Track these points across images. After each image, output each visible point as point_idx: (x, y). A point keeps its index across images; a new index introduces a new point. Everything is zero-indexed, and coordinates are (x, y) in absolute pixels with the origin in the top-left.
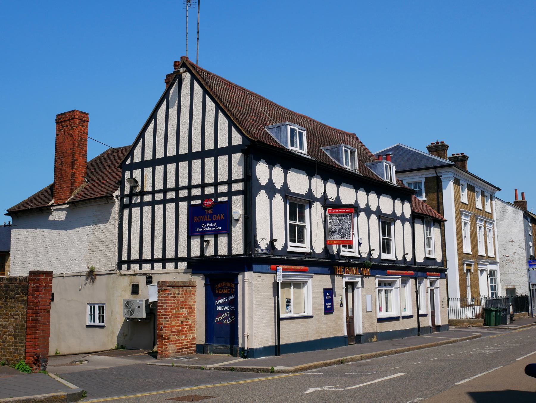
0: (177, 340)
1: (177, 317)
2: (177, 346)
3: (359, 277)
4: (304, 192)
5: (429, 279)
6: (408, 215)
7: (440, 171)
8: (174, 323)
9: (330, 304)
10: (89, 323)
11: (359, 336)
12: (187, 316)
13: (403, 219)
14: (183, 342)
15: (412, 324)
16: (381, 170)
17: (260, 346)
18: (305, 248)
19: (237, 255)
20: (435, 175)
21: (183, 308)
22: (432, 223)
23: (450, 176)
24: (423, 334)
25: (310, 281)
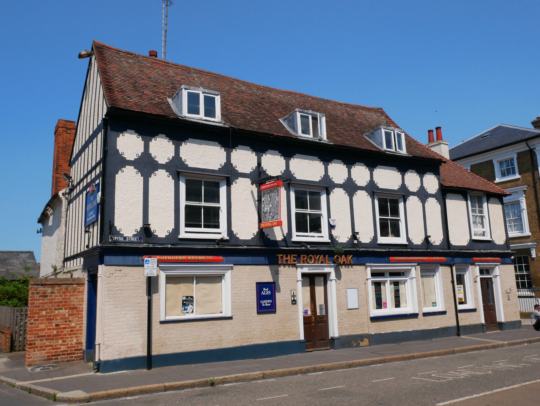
0: (47, 346)
1: (47, 320)
2: (47, 353)
3: (331, 267)
4: (396, 187)
5: (479, 265)
7: (532, 143)
8: (42, 326)
10: (162, 319)
11: (333, 339)
12: (69, 318)
13: (423, 195)
14: (60, 348)
15: (449, 321)
16: (379, 139)
17: (116, 357)
18: (220, 233)
20: (528, 148)
21: (61, 309)
22: (485, 199)
24: (465, 334)
25: (228, 274)
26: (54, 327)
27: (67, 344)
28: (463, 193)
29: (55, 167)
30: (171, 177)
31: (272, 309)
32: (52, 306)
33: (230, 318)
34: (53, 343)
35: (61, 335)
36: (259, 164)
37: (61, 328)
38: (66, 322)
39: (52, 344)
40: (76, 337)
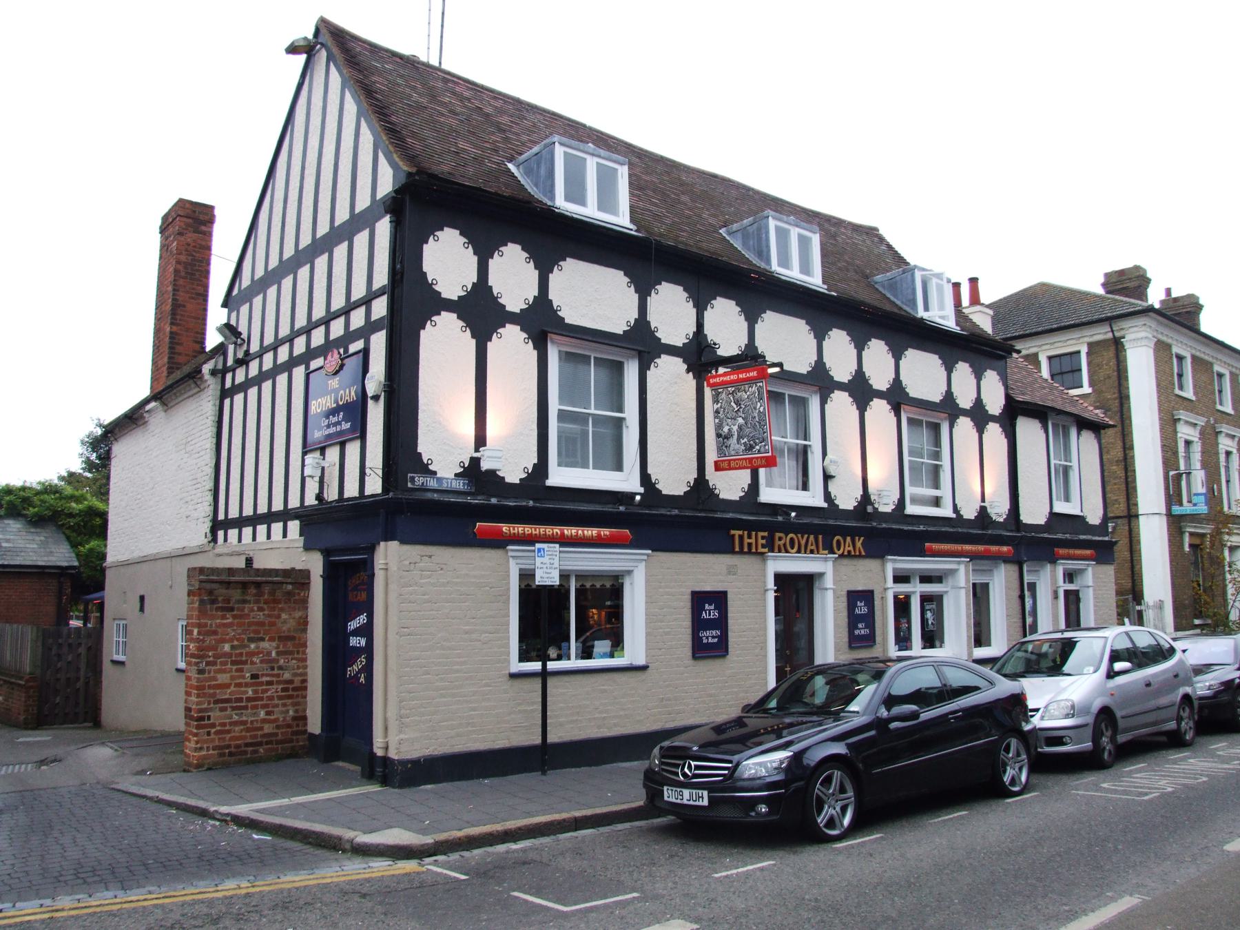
6: (995, 403)
8: (223, 678)
9: (857, 611)
12: (278, 661)
13: (979, 416)
16: (910, 291)
19: (372, 496)
20: (1110, 335)
21: (263, 639)
23: (1143, 334)
26: (249, 680)
27: (276, 720)
28: (1040, 413)
29: (168, 307)
30: (531, 343)
31: (720, 649)
32: (244, 632)
33: (643, 668)
34: (247, 716)
35: (262, 699)
36: (700, 325)
37: (262, 684)
38: (273, 669)
39: (244, 718)
40: (294, 704)
